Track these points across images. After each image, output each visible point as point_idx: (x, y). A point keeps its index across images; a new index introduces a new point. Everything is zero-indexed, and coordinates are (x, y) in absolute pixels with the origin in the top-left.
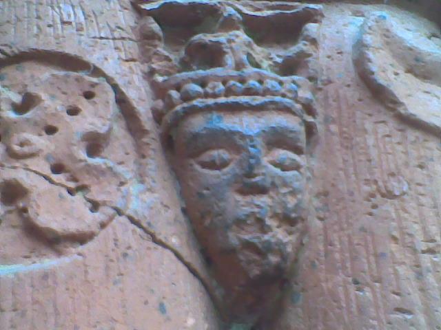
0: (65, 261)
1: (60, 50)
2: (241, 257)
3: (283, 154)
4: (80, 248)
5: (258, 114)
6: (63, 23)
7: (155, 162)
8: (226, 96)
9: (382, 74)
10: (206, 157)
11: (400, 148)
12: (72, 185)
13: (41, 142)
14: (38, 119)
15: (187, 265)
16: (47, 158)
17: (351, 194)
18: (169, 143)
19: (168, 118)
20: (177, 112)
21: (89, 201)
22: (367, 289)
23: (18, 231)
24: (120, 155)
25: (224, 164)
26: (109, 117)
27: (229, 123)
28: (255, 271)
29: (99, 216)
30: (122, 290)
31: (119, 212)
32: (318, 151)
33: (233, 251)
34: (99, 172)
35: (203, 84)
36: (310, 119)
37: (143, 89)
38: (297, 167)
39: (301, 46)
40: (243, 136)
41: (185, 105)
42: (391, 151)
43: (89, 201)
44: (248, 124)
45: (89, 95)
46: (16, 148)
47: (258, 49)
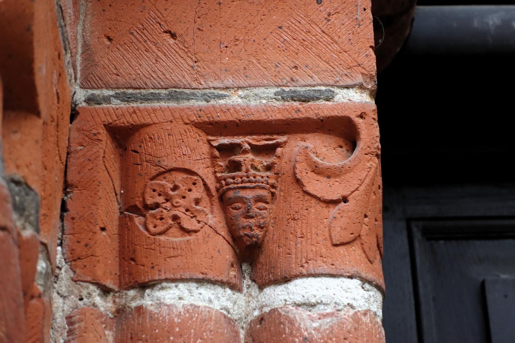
1: (184, 167)
2: (244, 239)
3: (261, 205)
4: (197, 234)
5: (252, 190)
8: (241, 183)
9: (301, 174)
10: (233, 206)
11: (301, 203)
12: (192, 215)
13: (182, 201)
14: (180, 194)
15: (227, 241)
16: (184, 207)
17: (283, 219)
19: (221, 191)
20: (224, 190)
21: (197, 220)
22: (281, 248)
23: (178, 229)
24: (205, 205)
25: (240, 208)
26: (201, 192)
27: (242, 194)
28: (248, 243)
29: (200, 225)
30: (208, 246)
31: (206, 224)
33: (242, 237)
36: (273, 190)
37: (212, 180)
38: (266, 209)
40: (246, 199)
41: (227, 187)
43: (197, 220)
44: (249, 194)
45: (194, 184)
46: (175, 204)
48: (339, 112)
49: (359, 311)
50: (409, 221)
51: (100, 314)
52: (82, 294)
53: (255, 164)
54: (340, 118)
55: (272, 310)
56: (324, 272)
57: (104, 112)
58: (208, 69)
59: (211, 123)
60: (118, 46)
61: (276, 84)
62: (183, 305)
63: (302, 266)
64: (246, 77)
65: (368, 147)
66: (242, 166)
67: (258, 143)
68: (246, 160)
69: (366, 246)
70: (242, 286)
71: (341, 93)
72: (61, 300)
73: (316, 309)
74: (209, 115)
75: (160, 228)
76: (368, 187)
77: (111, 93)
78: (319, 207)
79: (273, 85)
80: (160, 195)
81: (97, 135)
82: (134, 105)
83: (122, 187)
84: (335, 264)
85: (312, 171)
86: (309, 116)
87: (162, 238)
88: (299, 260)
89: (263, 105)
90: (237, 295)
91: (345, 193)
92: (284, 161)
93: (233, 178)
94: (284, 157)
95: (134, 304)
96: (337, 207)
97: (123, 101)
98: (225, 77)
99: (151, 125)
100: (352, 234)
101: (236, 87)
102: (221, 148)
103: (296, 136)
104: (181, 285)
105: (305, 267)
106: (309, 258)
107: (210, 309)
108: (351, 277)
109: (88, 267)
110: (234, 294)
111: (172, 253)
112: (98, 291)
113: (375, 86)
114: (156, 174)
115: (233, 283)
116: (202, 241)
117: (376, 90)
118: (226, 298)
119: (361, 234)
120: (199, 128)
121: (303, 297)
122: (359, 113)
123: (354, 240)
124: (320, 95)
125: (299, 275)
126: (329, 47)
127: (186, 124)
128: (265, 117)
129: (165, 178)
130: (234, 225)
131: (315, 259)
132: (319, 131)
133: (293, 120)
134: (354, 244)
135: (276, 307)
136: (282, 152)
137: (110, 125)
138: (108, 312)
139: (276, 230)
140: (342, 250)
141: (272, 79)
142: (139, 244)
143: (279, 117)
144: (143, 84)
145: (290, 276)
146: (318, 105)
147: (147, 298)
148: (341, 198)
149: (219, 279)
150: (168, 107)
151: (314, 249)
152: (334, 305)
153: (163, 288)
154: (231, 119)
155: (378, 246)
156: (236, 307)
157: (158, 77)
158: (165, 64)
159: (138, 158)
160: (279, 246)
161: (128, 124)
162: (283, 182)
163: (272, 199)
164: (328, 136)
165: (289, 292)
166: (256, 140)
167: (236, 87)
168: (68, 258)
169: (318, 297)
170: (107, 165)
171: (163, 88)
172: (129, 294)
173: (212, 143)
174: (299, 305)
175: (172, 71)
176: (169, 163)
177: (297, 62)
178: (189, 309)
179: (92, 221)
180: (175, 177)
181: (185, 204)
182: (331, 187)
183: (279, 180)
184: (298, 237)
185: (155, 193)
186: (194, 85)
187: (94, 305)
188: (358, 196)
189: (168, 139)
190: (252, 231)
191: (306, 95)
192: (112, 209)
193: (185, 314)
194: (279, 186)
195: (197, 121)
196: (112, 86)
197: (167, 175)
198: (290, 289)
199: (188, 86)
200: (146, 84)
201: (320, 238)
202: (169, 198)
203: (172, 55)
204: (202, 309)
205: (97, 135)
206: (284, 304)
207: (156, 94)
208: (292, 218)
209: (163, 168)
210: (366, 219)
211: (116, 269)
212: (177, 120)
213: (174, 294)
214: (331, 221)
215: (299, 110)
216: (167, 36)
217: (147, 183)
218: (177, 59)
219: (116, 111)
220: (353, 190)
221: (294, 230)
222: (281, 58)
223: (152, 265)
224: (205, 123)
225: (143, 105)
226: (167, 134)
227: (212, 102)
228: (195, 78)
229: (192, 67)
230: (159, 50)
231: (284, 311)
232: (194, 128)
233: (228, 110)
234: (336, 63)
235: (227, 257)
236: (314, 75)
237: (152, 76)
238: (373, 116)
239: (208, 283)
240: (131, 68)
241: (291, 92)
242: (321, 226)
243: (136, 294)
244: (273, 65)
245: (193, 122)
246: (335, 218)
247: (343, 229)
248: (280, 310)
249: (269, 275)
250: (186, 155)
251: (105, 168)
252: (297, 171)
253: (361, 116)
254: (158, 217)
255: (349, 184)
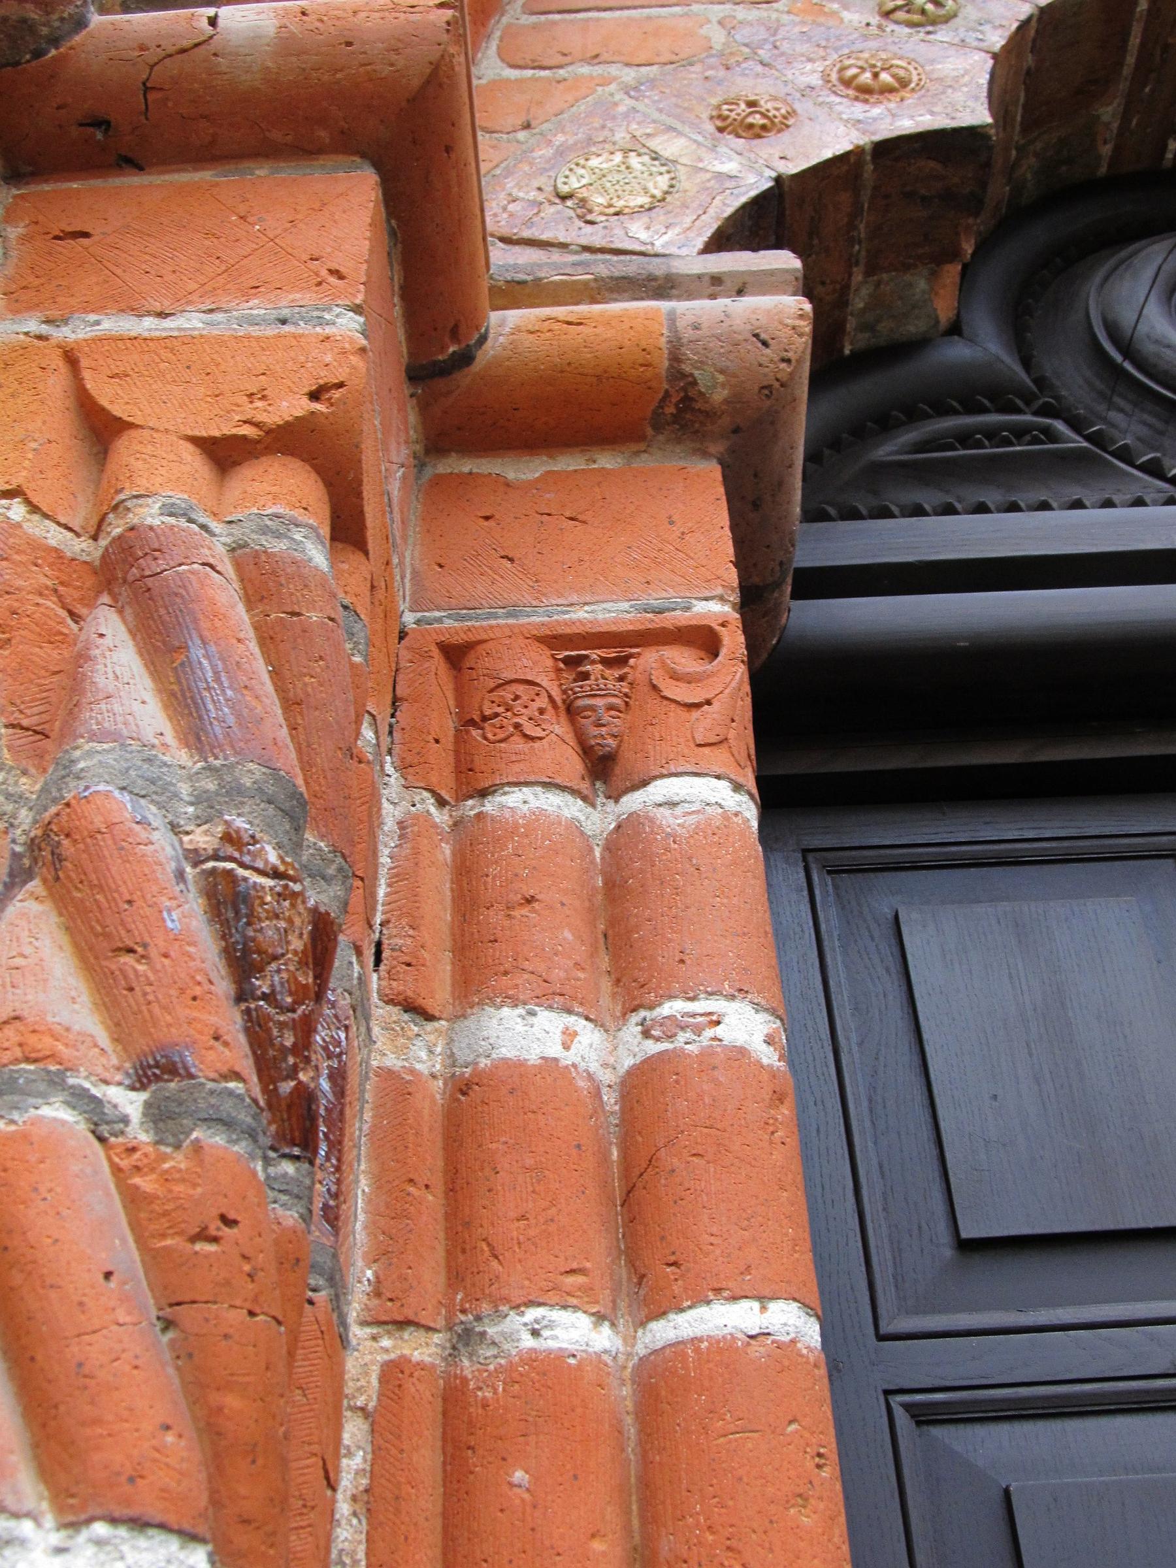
3: (613, 713)
13: (524, 711)
39: (626, 670)
44: (599, 702)
50: (805, 852)
59: (554, 637)
69: (734, 750)
73: (679, 807)
75: (501, 736)
82: (469, 624)
83: (457, 707)
91: (709, 696)
93: (581, 687)
102: (566, 661)
108: (718, 777)
112: (432, 801)
123: (721, 742)
143: (631, 628)
153: (505, 794)
155: (749, 756)
156: (589, 823)
174: (660, 805)
176: (508, 675)
186: (534, 603)
187: (428, 811)
197: (507, 687)
211: (452, 784)
216: (504, 561)
224: (547, 636)
253: (723, 625)
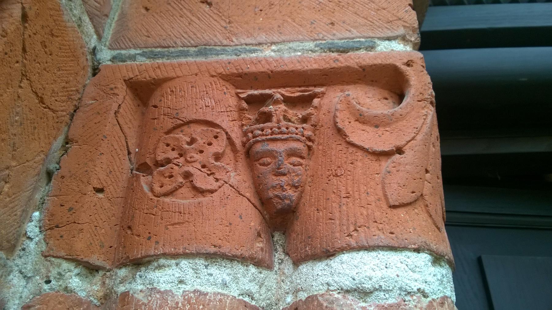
0: (206, 199)
1: (205, 119)
2: (274, 201)
3: (295, 159)
4: (212, 195)
6: (206, 106)
7: (242, 164)
8: (271, 135)
9: (342, 123)
10: (261, 161)
11: (345, 156)
13: (197, 156)
15: (253, 204)
16: (200, 163)
18: (248, 153)
20: (250, 143)
24: (228, 161)
27: (272, 146)
29: (218, 184)
31: (226, 183)
32: (313, 158)
34: (219, 168)
35: (262, 130)
36: (310, 144)
37: (238, 133)
38: (301, 165)
39: (310, 110)
40: (277, 152)
42: (340, 157)
43: (215, 178)
44: (280, 147)
45: (216, 137)
46: (189, 159)
47: (291, 112)
48: (383, 60)
49: (433, 300)
51: (77, 301)
52: (50, 274)
53: (288, 115)
54: (384, 66)
55: (309, 297)
56: (381, 244)
57: (126, 68)
58: (241, 29)
59: (240, 75)
60: (154, 14)
61: (312, 38)
62: (184, 292)
63: (350, 235)
64: (281, 33)
65: (421, 93)
66: (273, 116)
67: (293, 95)
68: (277, 110)
69: (431, 208)
70: (272, 261)
71: (383, 44)
72: (23, 282)
74: (238, 67)
76: (426, 136)
77: (138, 51)
78: (367, 160)
79: (308, 39)
80: (173, 150)
81: (114, 89)
82: (160, 61)
84: (395, 232)
85: (356, 121)
86: (349, 65)
87: (167, 200)
88: (345, 227)
89: (297, 57)
90: (265, 273)
91: (399, 143)
92: (322, 112)
94: (322, 108)
95: (122, 289)
96: (390, 161)
97: (149, 58)
98: (258, 34)
99: (174, 78)
100: (413, 192)
101: (270, 43)
102: (250, 100)
103: (335, 88)
104: (184, 263)
105: (353, 237)
106: (358, 224)
107: (222, 297)
108: (417, 250)
109: (65, 237)
110: (260, 273)
111: (176, 218)
113: (419, 39)
114: (172, 127)
115: (259, 258)
116: (218, 203)
117: (420, 44)
118: (248, 279)
119: (424, 193)
120: (227, 81)
121: (354, 279)
122: (406, 61)
124: (361, 45)
125: (346, 247)
126: (366, 6)
127: (213, 76)
128: (300, 68)
129: (182, 131)
130: (261, 184)
131: (367, 225)
132: (360, 81)
133: (331, 70)
134: (417, 206)
135: (315, 293)
136: (320, 103)
137: (130, 81)
138: (92, 298)
139: (314, 189)
140: (401, 213)
141: (307, 34)
142: (139, 208)
143: (315, 66)
144: (172, 43)
145: (334, 249)
146: (358, 54)
147: (139, 281)
148: (394, 149)
149: (239, 253)
150: (195, 61)
151: (365, 213)
152: (398, 292)
153: (160, 267)
154: (263, 70)
156: (263, 290)
157: (189, 37)
158: (197, 26)
159: (157, 113)
160: (318, 210)
161: (149, 79)
162: (321, 134)
163: (309, 154)
164: (371, 87)
165: (333, 271)
166: (290, 91)
167: (270, 43)
168: (44, 226)
169: (374, 280)
170: (119, 119)
171: (192, 46)
172: (119, 274)
173: (240, 95)
175: (204, 32)
177: (334, 19)
178: (191, 297)
179: (85, 180)
180: (194, 130)
181: (202, 159)
182: (380, 137)
183: (317, 132)
184: (342, 196)
185: (169, 148)
188: (416, 146)
189: (190, 91)
190: (284, 191)
191: (345, 46)
192: (120, 169)
193: (184, 305)
194: (317, 139)
195: (224, 73)
196: (140, 46)
197: (185, 128)
198: (335, 267)
199: (219, 44)
200: (176, 43)
201: (372, 198)
202: (183, 153)
203: (205, 18)
204: (210, 297)
205: (114, 89)
206: (326, 289)
207: (184, 51)
208: (334, 174)
209: (181, 120)
210: (428, 175)
212: (202, 73)
213: (173, 275)
214: (384, 176)
215: (337, 60)
217: (161, 137)
218: (211, 22)
219: (139, 68)
220: (409, 139)
221: (337, 188)
222: (316, 16)
223: (149, 235)
224: (233, 74)
225: (169, 61)
226: (190, 86)
227: (243, 56)
228: (227, 36)
229: (225, 28)
230: (193, 16)
231: (327, 300)
232: (221, 81)
233: (259, 61)
234: (374, 18)
235: (252, 224)
236: (352, 29)
237: (183, 36)
238: (422, 64)
239: (223, 259)
240: (163, 31)
241: (328, 44)
242: (372, 183)
243: (127, 274)
244: (309, 22)
245: (220, 74)
246: (389, 172)
247: (402, 186)
248: (320, 299)
249: (306, 248)
250: (209, 106)
251: (117, 123)
252: (338, 120)
253: (408, 64)
254: (167, 175)
255: (403, 133)
